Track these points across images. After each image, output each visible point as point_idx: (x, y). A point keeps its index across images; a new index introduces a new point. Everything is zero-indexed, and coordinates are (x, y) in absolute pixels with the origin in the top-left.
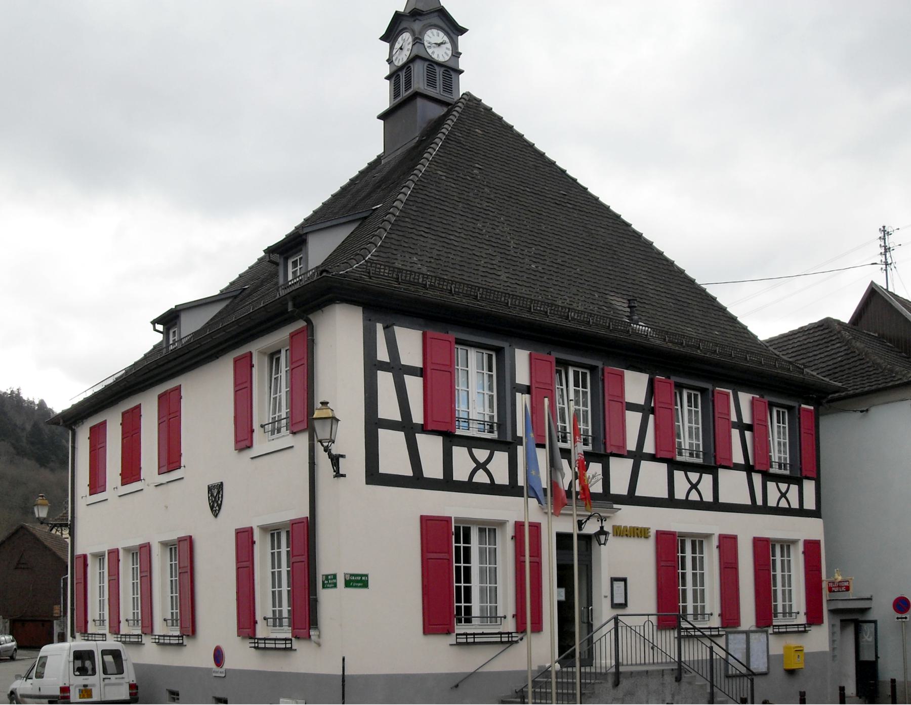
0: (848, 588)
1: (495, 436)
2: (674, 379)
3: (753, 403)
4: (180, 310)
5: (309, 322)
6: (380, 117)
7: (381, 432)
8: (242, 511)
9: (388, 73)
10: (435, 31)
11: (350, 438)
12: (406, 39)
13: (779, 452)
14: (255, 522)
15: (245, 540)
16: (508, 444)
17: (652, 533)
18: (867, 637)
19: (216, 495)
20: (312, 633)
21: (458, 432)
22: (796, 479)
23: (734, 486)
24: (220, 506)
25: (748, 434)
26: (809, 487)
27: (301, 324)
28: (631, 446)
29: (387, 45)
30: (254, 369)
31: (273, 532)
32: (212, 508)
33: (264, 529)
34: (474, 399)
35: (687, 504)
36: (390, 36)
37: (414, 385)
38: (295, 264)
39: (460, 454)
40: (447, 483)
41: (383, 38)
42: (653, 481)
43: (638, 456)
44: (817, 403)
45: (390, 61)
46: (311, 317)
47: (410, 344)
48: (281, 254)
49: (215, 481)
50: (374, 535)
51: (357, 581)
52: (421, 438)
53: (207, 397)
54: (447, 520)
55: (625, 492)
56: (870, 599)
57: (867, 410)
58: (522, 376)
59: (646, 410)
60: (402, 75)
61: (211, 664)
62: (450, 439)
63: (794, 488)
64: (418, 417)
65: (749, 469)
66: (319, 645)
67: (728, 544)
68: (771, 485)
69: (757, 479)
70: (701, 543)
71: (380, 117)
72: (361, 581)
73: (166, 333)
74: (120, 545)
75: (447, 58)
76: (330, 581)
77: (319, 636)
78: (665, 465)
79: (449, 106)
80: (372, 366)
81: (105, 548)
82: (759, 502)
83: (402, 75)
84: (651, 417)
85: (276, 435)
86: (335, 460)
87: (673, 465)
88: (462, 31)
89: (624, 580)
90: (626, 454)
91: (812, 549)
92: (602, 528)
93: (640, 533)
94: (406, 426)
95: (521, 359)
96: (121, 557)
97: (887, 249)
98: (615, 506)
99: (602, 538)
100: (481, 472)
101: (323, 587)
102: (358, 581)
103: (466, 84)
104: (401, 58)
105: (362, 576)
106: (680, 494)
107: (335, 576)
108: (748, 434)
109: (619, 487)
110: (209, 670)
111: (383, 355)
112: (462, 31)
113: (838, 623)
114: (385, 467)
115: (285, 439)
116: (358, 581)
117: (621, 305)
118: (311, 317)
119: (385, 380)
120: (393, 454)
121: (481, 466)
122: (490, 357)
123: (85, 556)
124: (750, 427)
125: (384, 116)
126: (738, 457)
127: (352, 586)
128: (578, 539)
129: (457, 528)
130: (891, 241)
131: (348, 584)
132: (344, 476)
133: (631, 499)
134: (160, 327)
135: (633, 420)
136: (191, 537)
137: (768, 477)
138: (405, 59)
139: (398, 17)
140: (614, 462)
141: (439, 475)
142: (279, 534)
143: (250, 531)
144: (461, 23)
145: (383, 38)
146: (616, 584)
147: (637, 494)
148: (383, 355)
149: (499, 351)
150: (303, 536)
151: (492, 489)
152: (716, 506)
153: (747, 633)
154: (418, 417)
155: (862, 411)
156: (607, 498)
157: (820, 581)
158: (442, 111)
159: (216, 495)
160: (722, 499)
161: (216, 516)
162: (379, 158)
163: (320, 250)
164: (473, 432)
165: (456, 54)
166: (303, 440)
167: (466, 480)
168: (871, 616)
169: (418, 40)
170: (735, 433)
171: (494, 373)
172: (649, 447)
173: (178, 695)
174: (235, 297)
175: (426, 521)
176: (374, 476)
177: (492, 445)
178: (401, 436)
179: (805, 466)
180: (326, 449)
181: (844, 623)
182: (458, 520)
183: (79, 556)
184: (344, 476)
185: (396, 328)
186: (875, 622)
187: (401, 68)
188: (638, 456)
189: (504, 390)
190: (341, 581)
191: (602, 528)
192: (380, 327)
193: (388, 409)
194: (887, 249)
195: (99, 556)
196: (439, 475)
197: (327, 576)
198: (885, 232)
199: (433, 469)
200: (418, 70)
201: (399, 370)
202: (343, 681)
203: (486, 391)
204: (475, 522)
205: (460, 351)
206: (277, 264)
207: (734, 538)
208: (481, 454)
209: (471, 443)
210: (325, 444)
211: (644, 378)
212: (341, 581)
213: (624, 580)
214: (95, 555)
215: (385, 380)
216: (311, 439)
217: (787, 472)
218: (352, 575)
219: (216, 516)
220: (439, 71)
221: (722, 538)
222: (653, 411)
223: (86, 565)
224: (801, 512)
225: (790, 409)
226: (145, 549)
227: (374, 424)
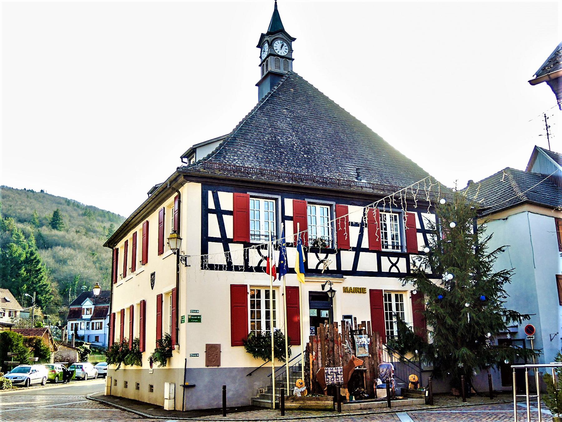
6: (256, 85)
9: (260, 63)
10: (276, 42)
21: (251, 242)
27: (176, 194)
28: (353, 243)
29: (260, 49)
35: (389, 274)
36: (260, 46)
37: (228, 220)
41: (258, 47)
42: (368, 261)
47: (227, 200)
48: (187, 157)
49: (152, 272)
57: (507, 219)
64: (230, 234)
70: (401, 296)
71: (256, 85)
72: (197, 319)
75: (286, 54)
78: (375, 254)
80: (205, 211)
88: (294, 39)
92: (331, 288)
98: (344, 277)
109: (347, 265)
111: (211, 205)
112: (294, 39)
119: (213, 219)
120: (216, 253)
123: (114, 314)
129: (385, 295)
131: (190, 320)
133: (354, 272)
136: (144, 300)
139: (263, 36)
144: (292, 36)
145: (258, 47)
147: (336, 269)
148: (211, 205)
154: (230, 234)
155: (504, 219)
165: (291, 51)
172: (365, 244)
175: (234, 288)
178: (220, 245)
185: (220, 193)
188: (358, 250)
191: (331, 288)
192: (210, 193)
193: (214, 231)
194: (548, 127)
199: (238, 259)
201: (219, 213)
210: (455, 247)
212: (186, 319)
215: (213, 219)
226: (132, 308)
227: (206, 239)
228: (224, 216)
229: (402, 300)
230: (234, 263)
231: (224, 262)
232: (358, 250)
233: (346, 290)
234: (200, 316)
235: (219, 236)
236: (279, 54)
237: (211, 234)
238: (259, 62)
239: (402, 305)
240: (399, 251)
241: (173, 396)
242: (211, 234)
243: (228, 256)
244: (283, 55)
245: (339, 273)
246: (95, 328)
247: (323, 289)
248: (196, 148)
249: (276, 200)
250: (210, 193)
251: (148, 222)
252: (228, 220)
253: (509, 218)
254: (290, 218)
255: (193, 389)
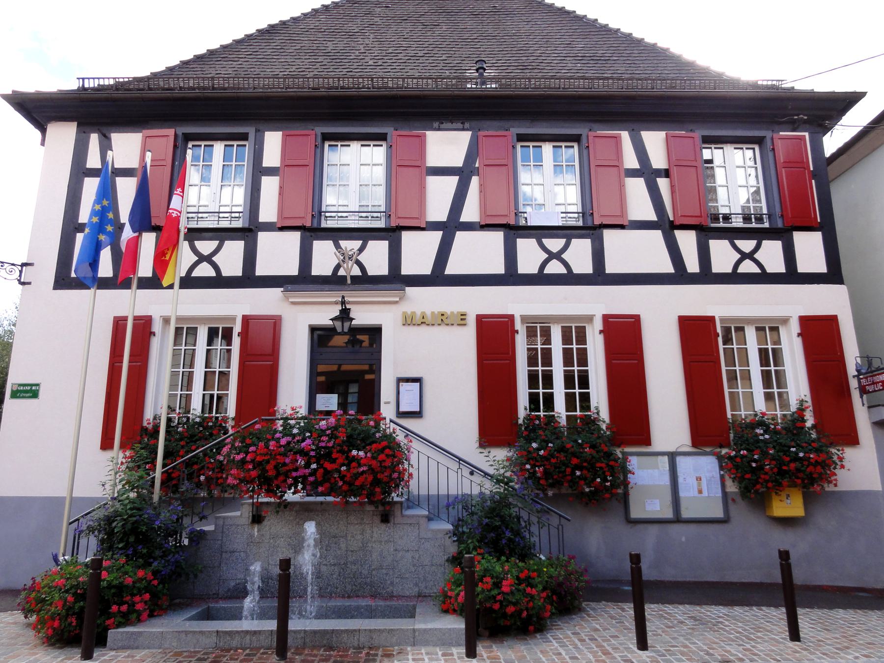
42: (478, 252)
51: (26, 392)
54: (711, 320)
90: (423, 226)
100: (205, 265)
105: (32, 385)
127: (19, 397)
128: (735, 331)
133: (438, 277)
146: (404, 386)
151: (570, 279)
153: (672, 456)
160: (801, 269)
167: (536, 272)
175: (127, 317)
182: (722, 320)
188: (451, 227)
204: (750, 321)
215: (91, 186)
218: (20, 385)
221: (805, 321)
229: (778, 361)
230: (802, 267)
231: (668, 267)
232: (451, 227)
233: (409, 321)
234: (38, 385)
235: (653, 217)
239: (780, 375)
240: (766, 225)
245: (396, 279)
249: (754, 149)
254: (271, 172)
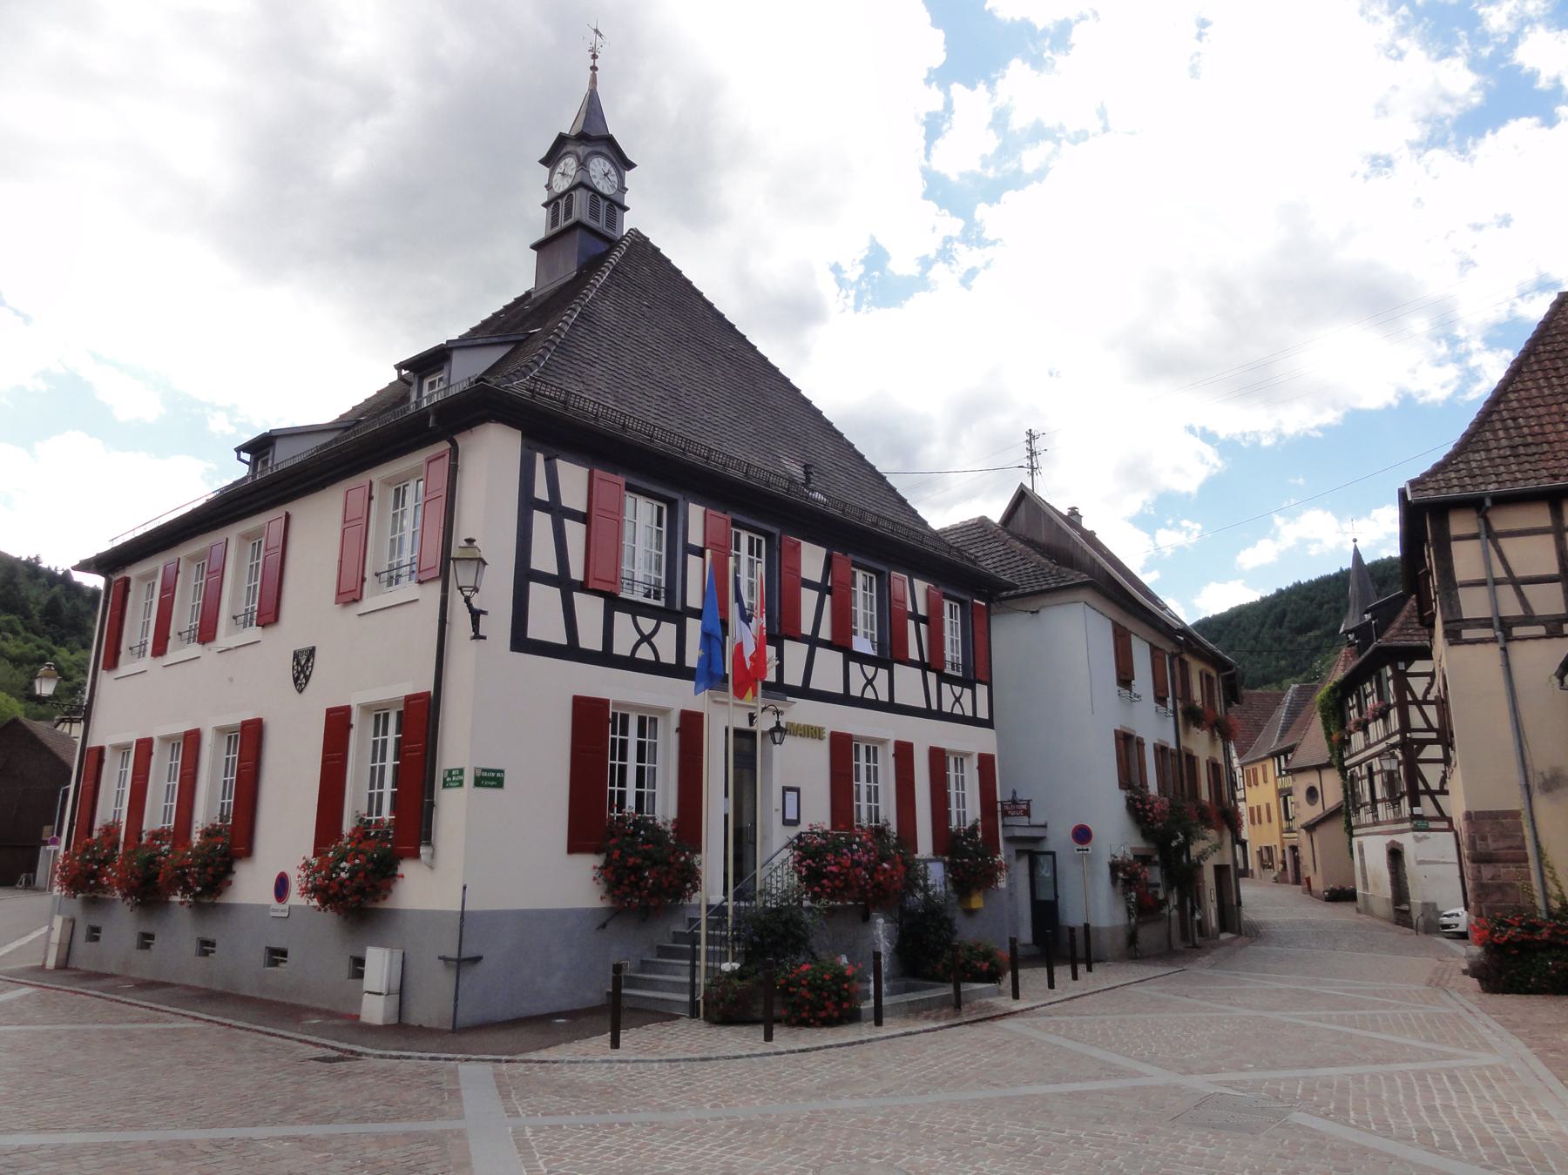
0: (1027, 813)
1: (661, 603)
2: (851, 556)
3: (928, 592)
4: (276, 437)
5: (454, 444)
6: (534, 247)
7: (533, 586)
8: (327, 691)
10: (601, 160)
11: (496, 592)
12: (569, 164)
13: (952, 652)
14: (355, 700)
15: (338, 723)
16: (675, 614)
17: (827, 735)
18: (1045, 872)
19: (303, 665)
20: (423, 850)
21: (622, 595)
22: (968, 682)
23: (909, 685)
24: (307, 678)
25: (922, 626)
26: (982, 690)
27: (444, 446)
28: (806, 629)
29: (546, 170)
30: (373, 503)
31: (379, 715)
32: (296, 680)
33: (366, 708)
34: (640, 561)
36: (550, 160)
37: (575, 532)
38: (432, 385)
39: (622, 620)
40: (606, 658)
43: (813, 642)
44: (989, 600)
45: (549, 187)
46: (456, 437)
47: (573, 482)
49: (307, 645)
50: (508, 720)
52: (579, 598)
53: (317, 525)
55: (799, 684)
56: (1045, 826)
58: (696, 538)
59: (822, 589)
60: (562, 203)
61: (268, 897)
62: (614, 603)
63: (968, 692)
64: (577, 573)
65: (923, 666)
66: (431, 867)
67: (904, 752)
68: (945, 687)
69: (932, 678)
71: (534, 247)
72: (495, 779)
73: (253, 465)
74: (156, 732)
76: (454, 779)
77: (433, 856)
79: (613, 244)
80: (528, 505)
81: (132, 737)
82: (934, 707)
83: (562, 203)
84: (828, 597)
85: (394, 587)
86: (476, 615)
87: (851, 656)
89: (797, 790)
91: (986, 763)
93: (814, 733)
94: (562, 582)
95: (696, 513)
96: (155, 750)
97: (1033, 453)
99: (777, 735)
101: (444, 786)
102: (490, 779)
103: (629, 222)
104: (561, 185)
106: (855, 691)
107: (461, 771)
108: (922, 626)
110: (267, 907)
113: (1013, 853)
114: (534, 632)
115: (408, 589)
116: (490, 779)
117: (797, 471)
118: (456, 437)
119: (542, 523)
121: (646, 638)
122: (660, 509)
123: (101, 750)
124: (925, 620)
125: (537, 247)
126: (914, 654)
129: (615, 715)
130: (1037, 445)
131: (479, 782)
132: (484, 638)
133: (805, 692)
134: (246, 456)
135: (809, 598)
137: (943, 678)
138: (567, 186)
139: (562, 140)
140: (788, 645)
141: (597, 646)
142: (386, 716)
143: (347, 711)
148: (541, 492)
149: (672, 504)
150: (420, 719)
152: (891, 707)
156: (779, 689)
157: (948, 814)
158: (603, 247)
159: (303, 665)
161: (300, 691)
162: (528, 294)
163: (464, 371)
164: (638, 597)
165: (623, 189)
166: (435, 589)
168: (1049, 846)
169: (583, 165)
170: (911, 624)
171: (664, 529)
172: (825, 633)
173: (213, 945)
174: (347, 429)
176: (521, 642)
177: (659, 615)
178: (556, 593)
179: (976, 671)
180: (467, 600)
181: (1019, 853)
182: (616, 704)
183: (91, 749)
184: (484, 638)
185: (559, 462)
186: (1053, 854)
187: (561, 196)
189: (675, 549)
190: (468, 778)
192: (540, 458)
193: (543, 558)
194: (1033, 453)
195: (123, 749)
196: (597, 646)
197: (450, 771)
198: (1031, 437)
199: (591, 639)
200: (580, 197)
202: (462, 917)
203: (654, 551)
205: (629, 500)
206: (410, 384)
207: (910, 746)
208: (647, 624)
209: (635, 609)
211: (822, 551)
212: (468, 778)
213: (797, 790)
214: (116, 748)
215: (542, 523)
216: (445, 589)
217: (960, 674)
219: (300, 691)
220: (603, 204)
222: (830, 591)
223: (101, 761)
224: (974, 721)
225: (962, 603)
226: (192, 740)
227: (525, 575)
228: (568, 523)
231: (561, 639)
236: (600, 188)
237: (536, 564)
238: (544, 197)
241: (396, 985)
242: (536, 564)
243: (1521, 595)
244: (606, 192)
246: (1487, 872)
247: (751, 724)
248: (451, 349)
250: (540, 458)
251: (288, 517)
252: (575, 532)
253: (1042, 612)
255: (480, 966)
